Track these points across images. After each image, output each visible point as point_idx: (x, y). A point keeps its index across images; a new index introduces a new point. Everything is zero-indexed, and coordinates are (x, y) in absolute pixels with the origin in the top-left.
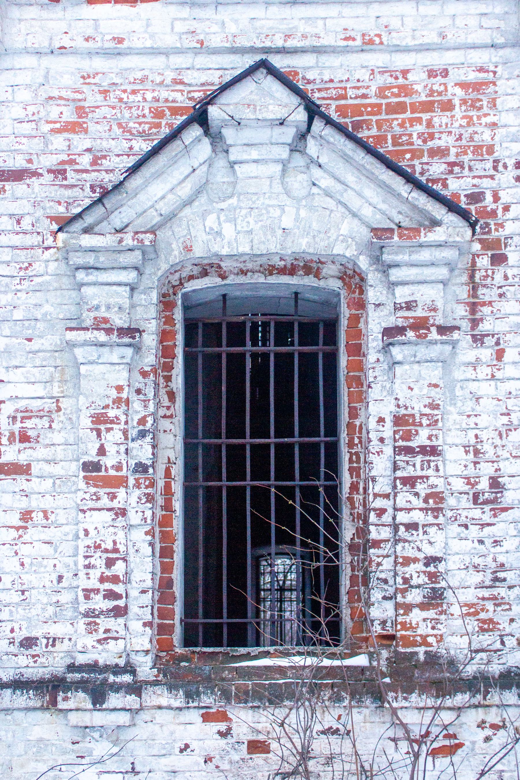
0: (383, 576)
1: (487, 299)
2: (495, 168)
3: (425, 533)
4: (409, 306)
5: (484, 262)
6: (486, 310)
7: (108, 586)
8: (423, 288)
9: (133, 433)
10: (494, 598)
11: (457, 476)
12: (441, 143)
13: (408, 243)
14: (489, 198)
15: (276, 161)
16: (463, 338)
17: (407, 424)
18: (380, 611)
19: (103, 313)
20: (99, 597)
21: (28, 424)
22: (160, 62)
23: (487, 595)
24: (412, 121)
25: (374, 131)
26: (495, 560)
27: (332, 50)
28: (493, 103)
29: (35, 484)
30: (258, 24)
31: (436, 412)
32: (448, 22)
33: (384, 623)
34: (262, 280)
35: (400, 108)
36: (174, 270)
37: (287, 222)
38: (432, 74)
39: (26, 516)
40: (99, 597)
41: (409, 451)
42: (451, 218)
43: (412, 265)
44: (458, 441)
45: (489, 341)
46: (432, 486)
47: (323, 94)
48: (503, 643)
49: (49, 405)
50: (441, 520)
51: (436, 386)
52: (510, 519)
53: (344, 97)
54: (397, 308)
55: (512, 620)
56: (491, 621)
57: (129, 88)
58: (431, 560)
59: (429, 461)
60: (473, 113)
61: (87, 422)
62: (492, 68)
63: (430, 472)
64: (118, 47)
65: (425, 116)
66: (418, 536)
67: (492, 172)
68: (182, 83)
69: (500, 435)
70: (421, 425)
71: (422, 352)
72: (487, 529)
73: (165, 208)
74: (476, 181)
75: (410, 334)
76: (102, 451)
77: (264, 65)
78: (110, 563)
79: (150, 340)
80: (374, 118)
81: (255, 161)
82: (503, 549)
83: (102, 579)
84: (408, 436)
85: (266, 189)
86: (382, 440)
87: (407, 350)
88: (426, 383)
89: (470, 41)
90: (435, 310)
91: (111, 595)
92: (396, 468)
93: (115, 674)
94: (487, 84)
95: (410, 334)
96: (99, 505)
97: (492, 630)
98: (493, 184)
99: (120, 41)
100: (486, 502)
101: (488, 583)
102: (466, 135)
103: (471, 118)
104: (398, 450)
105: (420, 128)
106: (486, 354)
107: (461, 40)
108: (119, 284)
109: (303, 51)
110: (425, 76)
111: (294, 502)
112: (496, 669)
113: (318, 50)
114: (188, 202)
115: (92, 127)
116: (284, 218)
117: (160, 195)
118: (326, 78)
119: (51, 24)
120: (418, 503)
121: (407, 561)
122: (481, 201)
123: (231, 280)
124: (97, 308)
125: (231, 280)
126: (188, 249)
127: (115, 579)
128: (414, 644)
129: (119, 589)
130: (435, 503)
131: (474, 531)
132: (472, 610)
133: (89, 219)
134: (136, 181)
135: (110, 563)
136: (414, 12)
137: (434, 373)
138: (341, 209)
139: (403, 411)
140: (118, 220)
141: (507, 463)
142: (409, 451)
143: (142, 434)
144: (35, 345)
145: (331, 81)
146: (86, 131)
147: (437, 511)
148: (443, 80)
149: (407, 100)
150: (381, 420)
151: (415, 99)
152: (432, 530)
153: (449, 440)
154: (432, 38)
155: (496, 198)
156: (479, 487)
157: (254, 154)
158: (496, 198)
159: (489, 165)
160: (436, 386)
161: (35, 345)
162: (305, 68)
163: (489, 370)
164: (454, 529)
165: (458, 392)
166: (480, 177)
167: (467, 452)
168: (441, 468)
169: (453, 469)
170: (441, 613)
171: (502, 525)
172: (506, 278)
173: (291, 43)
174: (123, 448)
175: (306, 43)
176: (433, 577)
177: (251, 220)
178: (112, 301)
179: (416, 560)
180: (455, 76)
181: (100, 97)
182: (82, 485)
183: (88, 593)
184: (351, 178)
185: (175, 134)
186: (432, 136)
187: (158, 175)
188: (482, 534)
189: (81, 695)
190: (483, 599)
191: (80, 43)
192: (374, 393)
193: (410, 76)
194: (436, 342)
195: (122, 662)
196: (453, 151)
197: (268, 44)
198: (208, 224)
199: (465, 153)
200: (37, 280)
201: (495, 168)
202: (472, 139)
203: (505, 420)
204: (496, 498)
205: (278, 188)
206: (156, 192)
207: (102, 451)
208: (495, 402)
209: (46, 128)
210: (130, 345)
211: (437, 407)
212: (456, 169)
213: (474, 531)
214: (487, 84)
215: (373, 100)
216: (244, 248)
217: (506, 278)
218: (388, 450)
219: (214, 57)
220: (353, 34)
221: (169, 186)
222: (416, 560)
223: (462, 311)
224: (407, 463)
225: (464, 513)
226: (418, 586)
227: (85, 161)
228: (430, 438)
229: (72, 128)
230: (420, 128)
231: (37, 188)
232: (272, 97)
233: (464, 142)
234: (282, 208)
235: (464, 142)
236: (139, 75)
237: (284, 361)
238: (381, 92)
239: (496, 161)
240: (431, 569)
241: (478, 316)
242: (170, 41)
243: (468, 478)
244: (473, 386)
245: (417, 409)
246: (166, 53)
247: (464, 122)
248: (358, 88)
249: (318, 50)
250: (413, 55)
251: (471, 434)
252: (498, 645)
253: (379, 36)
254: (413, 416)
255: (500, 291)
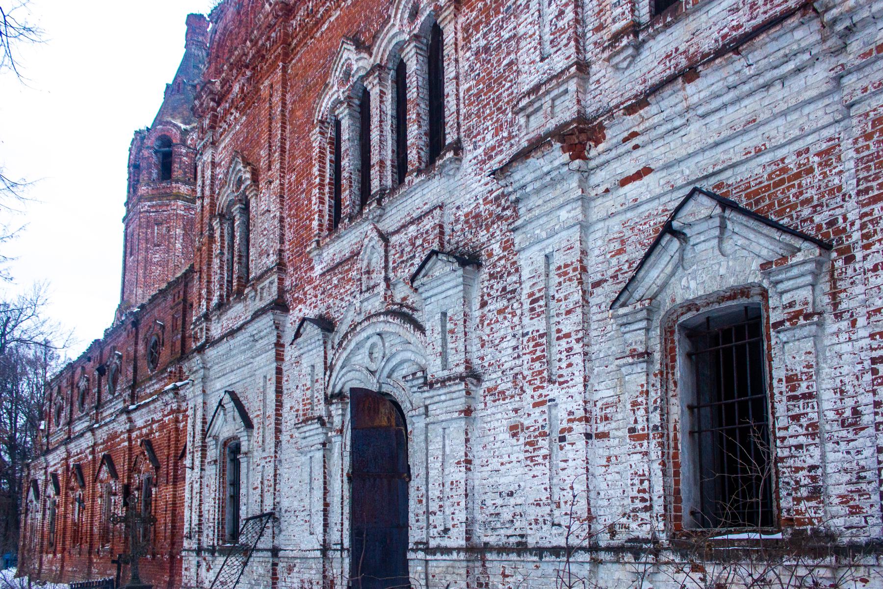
0: (786, 480)
1: (843, 287)
2: (844, 200)
3: (807, 450)
4: (791, 305)
5: (840, 263)
6: (843, 295)
7: (641, 495)
8: (799, 292)
9: (651, 409)
10: (858, 491)
11: (830, 410)
12: (808, 195)
13: (781, 267)
14: (841, 220)
15: (715, 238)
16: (829, 318)
17: (793, 380)
18: (785, 503)
19: (634, 347)
20: (637, 501)
21: (608, 411)
22: (655, 203)
23: (853, 489)
24: (788, 188)
25: (767, 202)
26: (858, 464)
27: (741, 163)
28: (839, 159)
29: (613, 442)
30: (699, 165)
31: (811, 370)
32: (805, 119)
33: (788, 510)
34: (717, 307)
35: (782, 182)
36: (669, 314)
37: (722, 271)
38: (799, 154)
39: (609, 459)
40: (637, 501)
41: (795, 398)
42: (806, 245)
43: (790, 279)
44: (829, 386)
45: (846, 316)
46: (810, 419)
47: (738, 190)
48: (866, 522)
49: (615, 399)
50: (817, 440)
51: (810, 353)
52: (867, 435)
53: (749, 187)
54: (785, 307)
55: (872, 506)
56: (858, 506)
57: (643, 222)
58: (812, 468)
59: (808, 403)
60: (827, 169)
61: (629, 406)
62: (837, 136)
63: (809, 410)
64: (636, 204)
65: (796, 182)
66: (803, 453)
67: (842, 203)
68: (667, 210)
69: (857, 378)
70: (801, 380)
71: (799, 333)
72: (851, 444)
73: (659, 282)
74: (830, 213)
75: (787, 324)
76: (636, 421)
77: (695, 190)
78: (642, 482)
79: (657, 356)
80: (766, 194)
81: (704, 241)
82: (863, 456)
83: (639, 491)
84: (793, 389)
85: (710, 255)
86: (781, 393)
87: (789, 334)
88: (804, 352)
89: (819, 125)
90: (807, 304)
91: (643, 500)
92: (788, 410)
93: (646, 543)
94: (834, 148)
95: (787, 324)
96: (635, 451)
97: (858, 513)
98: (843, 210)
99: (636, 200)
100: (850, 425)
101: (854, 480)
102: (823, 185)
103: (825, 173)
104: (790, 398)
105: (793, 191)
106: (844, 325)
107: (814, 126)
108: (640, 329)
109: (725, 169)
110: (794, 157)
111: (727, 439)
112: (862, 539)
113: (733, 166)
114: (673, 274)
115: (628, 249)
116: (721, 269)
117: (656, 275)
118: (739, 180)
119: (607, 204)
120: (802, 431)
121: (797, 470)
122: (835, 224)
123: (702, 310)
124: (631, 344)
125: (702, 310)
126: (673, 301)
127: (644, 491)
128: (804, 524)
129: (646, 496)
130: (814, 430)
131: (843, 446)
132: (844, 500)
133: (622, 300)
134: (642, 273)
135: (642, 482)
136: (784, 122)
137: (809, 345)
138: (752, 255)
139: (790, 373)
140: (637, 295)
141: (863, 396)
142: (795, 398)
143: (655, 409)
144: (609, 369)
145: (742, 180)
146: (625, 252)
147: (813, 435)
148: (806, 156)
149: (786, 176)
150: (780, 380)
151: (790, 173)
152: (812, 448)
153: (824, 387)
154: (796, 132)
155: (845, 219)
156: (845, 415)
157: (702, 238)
158: (845, 219)
159: (839, 199)
160: (810, 353)
161: (609, 369)
162: (728, 179)
163: (847, 336)
164: (830, 446)
165: (828, 354)
166: (834, 209)
167: (835, 393)
168: (816, 406)
169: (826, 405)
170: (820, 503)
171: (861, 440)
172: (855, 270)
173: (717, 168)
174: (645, 418)
175: (725, 165)
176: (814, 479)
177: (704, 275)
178: (637, 339)
179: (802, 469)
180: (814, 150)
181: (630, 232)
182: (628, 441)
183: (633, 499)
184: (751, 236)
185: (657, 242)
186: (801, 193)
187: (653, 266)
188: (848, 447)
189: (629, 555)
190: (852, 492)
191: (620, 208)
192: (775, 364)
193: (786, 161)
194: (805, 325)
195: (650, 537)
196: (816, 197)
197: (705, 173)
198: (683, 283)
199: (824, 196)
200: (609, 335)
201: (844, 200)
202: (827, 186)
203: (860, 367)
204: (856, 421)
205: (717, 252)
206: (653, 275)
207: (636, 421)
208: (852, 356)
209: (608, 256)
210: (644, 362)
211: (811, 366)
212: (818, 209)
213: (843, 446)
214: (834, 148)
215: (766, 183)
216: (701, 293)
217: (855, 270)
218: (784, 399)
219: (680, 191)
220: (749, 150)
221: (660, 270)
222: (802, 469)
223: (826, 300)
224: (794, 406)
225: (836, 434)
226: (805, 486)
227: (626, 267)
228: (808, 387)
229: (620, 252)
230: (793, 191)
231: (606, 287)
232: (702, 205)
233: (822, 190)
234: (719, 264)
235: (822, 190)
236: (647, 214)
237: (728, 352)
238: (770, 177)
239: (844, 195)
240: (813, 473)
241: (838, 300)
242: (658, 191)
243: (837, 410)
244: (837, 348)
245: (799, 370)
246: (658, 197)
247: (821, 177)
248: (756, 179)
249: (733, 166)
250: (787, 147)
251: (838, 380)
252: (863, 523)
253: (764, 145)
254: (796, 375)
255: (851, 280)
